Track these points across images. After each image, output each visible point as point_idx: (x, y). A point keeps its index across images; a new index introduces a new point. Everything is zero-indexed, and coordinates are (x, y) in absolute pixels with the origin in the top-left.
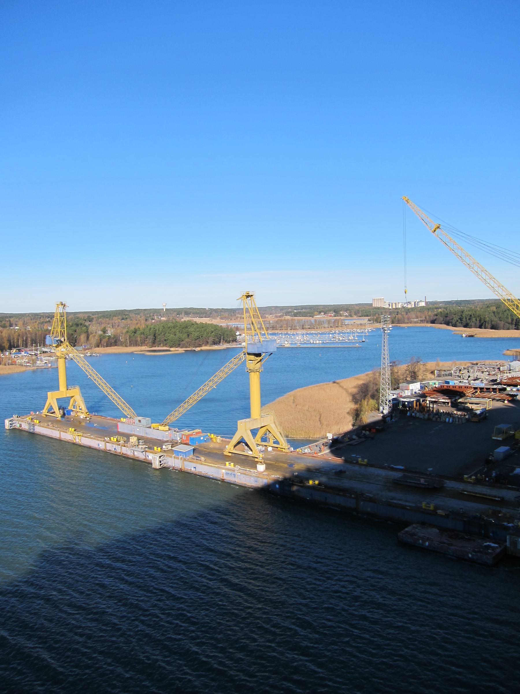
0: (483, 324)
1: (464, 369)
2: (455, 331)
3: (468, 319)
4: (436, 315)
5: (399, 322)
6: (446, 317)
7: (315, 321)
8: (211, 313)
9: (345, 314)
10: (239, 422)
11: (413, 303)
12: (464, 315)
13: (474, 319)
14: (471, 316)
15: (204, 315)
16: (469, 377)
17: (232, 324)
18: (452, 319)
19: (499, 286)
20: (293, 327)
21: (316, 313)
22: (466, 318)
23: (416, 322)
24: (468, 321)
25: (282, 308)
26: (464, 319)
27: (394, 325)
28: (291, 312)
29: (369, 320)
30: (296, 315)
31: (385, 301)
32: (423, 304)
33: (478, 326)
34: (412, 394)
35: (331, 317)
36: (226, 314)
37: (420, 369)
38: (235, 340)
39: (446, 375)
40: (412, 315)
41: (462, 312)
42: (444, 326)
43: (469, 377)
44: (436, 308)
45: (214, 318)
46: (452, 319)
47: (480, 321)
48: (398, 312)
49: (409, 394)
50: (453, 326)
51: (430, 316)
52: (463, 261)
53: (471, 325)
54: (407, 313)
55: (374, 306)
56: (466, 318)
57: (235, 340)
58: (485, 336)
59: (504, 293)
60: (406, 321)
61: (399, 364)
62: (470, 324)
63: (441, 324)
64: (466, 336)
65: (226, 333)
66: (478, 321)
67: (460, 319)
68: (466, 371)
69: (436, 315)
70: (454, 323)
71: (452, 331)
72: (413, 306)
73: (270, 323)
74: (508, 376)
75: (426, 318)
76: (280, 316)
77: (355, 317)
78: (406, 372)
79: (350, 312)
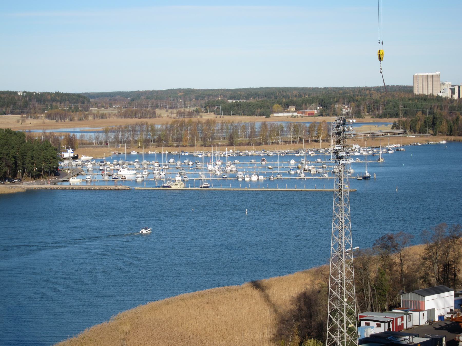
7: (264, 125)
8: (26, 104)
10: (427, 298)
15: (9, 109)
17: (62, 129)
20: (208, 142)
21: (276, 106)
25: (188, 94)
27: (452, 138)
28: (218, 104)
29: (395, 126)
30: (228, 110)
31: (442, 80)
34: (431, 322)
36: (63, 107)
38: (55, 172)
45: (33, 115)
49: (424, 322)
55: (416, 92)
57: (55, 172)
65: (30, 153)
73: (153, 130)
76: (191, 114)
77: (368, 118)
78: (423, 264)
79: (358, 106)
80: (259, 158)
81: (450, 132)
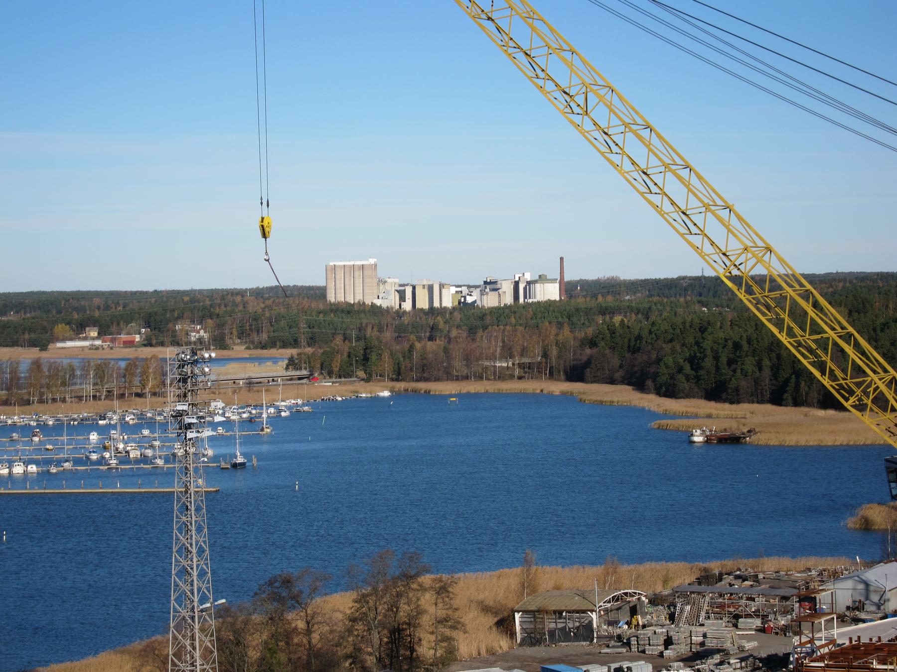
0: (787, 381)
1: (655, 601)
2: (666, 415)
3: (724, 360)
4: (593, 343)
5: (426, 372)
6: (634, 350)
9: (194, 336)
11: (507, 288)
12: (707, 345)
13: (749, 363)
14: (737, 346)
16: (668, 642)
18: (659, 360)
19: (707, 207)
21: (60, 328)
22: (716, 358)
23: (503, 375)
24: (725, 370)
26: (708, 363)
27: (401, 386)
29: (292, 363)
31: (381, 274)
32: (550, 292)
33: (768, 396)
35: (127, 347)
37: (420, 612)
39: (566, 635)
40: (490, 341)
41: (702, 330)
42: (624, 395)
43: (668, 642)
44: (604, 311)
46: (659, 360)
47: (776, 370)
48: (433, 328)
50: (659, 394)
51: (562, 347)
52: (538, 73)
53: (737, 389)
54: (472, 331)
55: (331, 298)
56: (716, 358)
58: (791, 440)
59: (734, 246)
60: (458, 365)
61: (314, 591)
62: (733, 384)
63: (612, 381)
64: (708, 441)
66: (767, 372)
67: (691, 360)
68: (662, 613)
69: (593, 343)
70: (664, 378)
71: (654, 416)
72: (508, 300)
74: (832, 642)
75: (545, 355)
77: (239, 350)
78: (350, 631)
79: (221, 326)
80: (27, 431)
81: (398, 375)
